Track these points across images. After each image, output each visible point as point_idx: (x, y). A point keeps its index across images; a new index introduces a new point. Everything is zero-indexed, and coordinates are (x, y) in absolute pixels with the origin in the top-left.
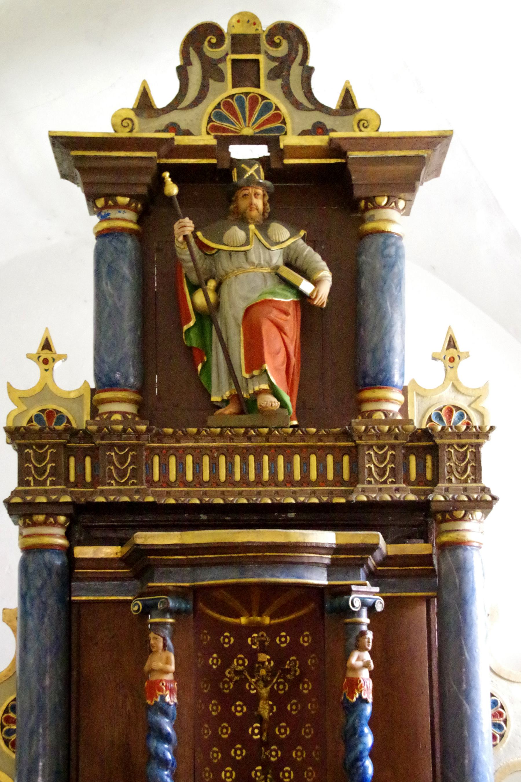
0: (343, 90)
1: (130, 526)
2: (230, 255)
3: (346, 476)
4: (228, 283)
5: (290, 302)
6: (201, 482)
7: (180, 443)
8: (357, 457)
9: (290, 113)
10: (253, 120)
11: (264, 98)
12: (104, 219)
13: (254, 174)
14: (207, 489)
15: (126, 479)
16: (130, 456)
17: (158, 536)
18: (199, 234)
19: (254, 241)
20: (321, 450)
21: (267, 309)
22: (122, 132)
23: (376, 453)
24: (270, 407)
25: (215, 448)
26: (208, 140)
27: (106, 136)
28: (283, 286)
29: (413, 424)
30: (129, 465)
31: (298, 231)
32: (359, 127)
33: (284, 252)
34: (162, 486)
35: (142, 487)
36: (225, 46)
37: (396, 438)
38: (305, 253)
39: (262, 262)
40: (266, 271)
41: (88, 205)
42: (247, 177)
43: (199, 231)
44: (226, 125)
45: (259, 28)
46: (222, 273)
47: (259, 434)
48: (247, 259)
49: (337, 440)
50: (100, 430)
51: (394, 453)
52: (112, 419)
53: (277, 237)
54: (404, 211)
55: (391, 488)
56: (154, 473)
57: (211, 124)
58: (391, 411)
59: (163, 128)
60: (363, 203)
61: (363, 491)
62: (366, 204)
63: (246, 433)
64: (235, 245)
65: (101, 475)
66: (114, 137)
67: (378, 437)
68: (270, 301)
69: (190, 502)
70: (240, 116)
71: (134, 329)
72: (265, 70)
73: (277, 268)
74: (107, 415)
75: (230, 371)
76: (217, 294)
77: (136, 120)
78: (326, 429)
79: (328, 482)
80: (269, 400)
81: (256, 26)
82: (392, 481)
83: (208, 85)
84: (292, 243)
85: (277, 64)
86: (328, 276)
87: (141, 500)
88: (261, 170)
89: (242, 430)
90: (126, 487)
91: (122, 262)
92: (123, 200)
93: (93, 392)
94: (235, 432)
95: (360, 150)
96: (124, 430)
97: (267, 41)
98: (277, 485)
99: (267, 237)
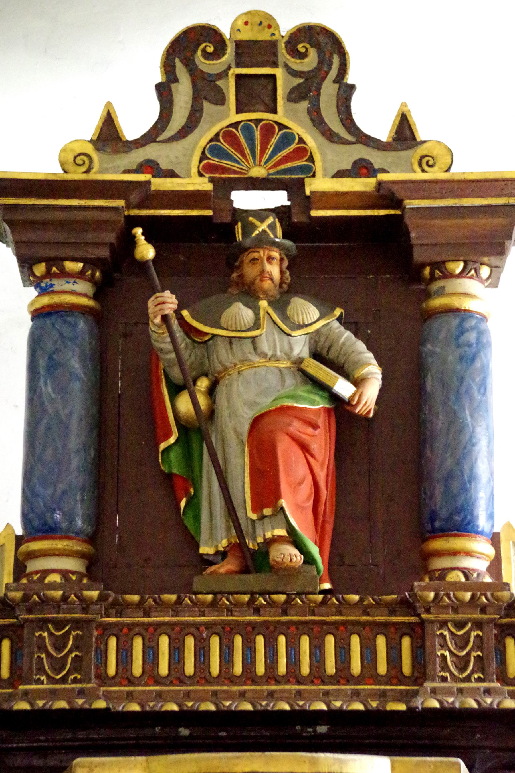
0: (397, 116)
1: (66, 748)
2: (231, 343)
3: (407, 669)
4: (227, 382)
5: (320, 409)
6: (182, 678)
7: (149, 617)
8: (423, 638)
9: (320, 147)
10: (266, 156)
11: (282, 126)
12: (43, 292)
13: (267, 230)
14: (191, 688)
15: (64, 672)
16: (71, 637)
17: (112, 763)
18: (185, 313)
19: (266, 323)
20: (368, 629)
21: (286, 419)
22: (75, 172)
23: (451, 633)
24: (289, 563)
25: (204, 625)
26: (200, 184)
27: (50, 178)
28: (309, 387)
29: (509, 590)
30: (70, 651)
31: (333, 310)
32: (420, 165)
33: (311, 338)
34: (120, 684)
35: (90, 685)
36: (226, 56)
37: (483, 610)
38: (342, 340)
39: (278, 353)
40: (284, 366)
41: (22, 272)
42: (257, 235)
43: (185, 309)
44: (226, 163)
45: (276, 33)
46: (220, 368)
47: (272, 604)
48: (255, 348)
49: (392, 613)
50: (26, 598)
51: (480, 633)
52: (46, 581)
53: (301, 317)
54: (490, 281)
55: (478, 689)
56: (109, 663)
57: (205, 162)
58: (474, 570)
59: (135, 167)
60: (427, 271)
61: (434, 691)
62: (432, 273)
63: (252, 601)
64: (239, 329)
65: (25, 667)
66: (62, 179)
67: (456, 610)
68: (289, 408)
69: (163, 709)
70: (247, 151)
71: (86, 448)
72: (283, 90)
73: (300, 361)
74: (39, 575)
75: (229, 510)
76: (211, 398)
77: (95, 156)
78: (376, 597)
79: (379, 678)
80: (287, 553)
81: (272, 30)
82: (479, 677)
83: (202, 109)
84: (323, 326)
85: (301, 81)
86: (376, 373)
87: (87, 706)
88: (278, 225)
89: (246, 598)
90: (63, 686)
91: (70, 353)
92: (70, 266)
93: (19, 541)
94: (234, 599)
95: (423, 198)
96: (65, 599)
97: (287, 51)
98: (299, 683)
99: (285, 318)
